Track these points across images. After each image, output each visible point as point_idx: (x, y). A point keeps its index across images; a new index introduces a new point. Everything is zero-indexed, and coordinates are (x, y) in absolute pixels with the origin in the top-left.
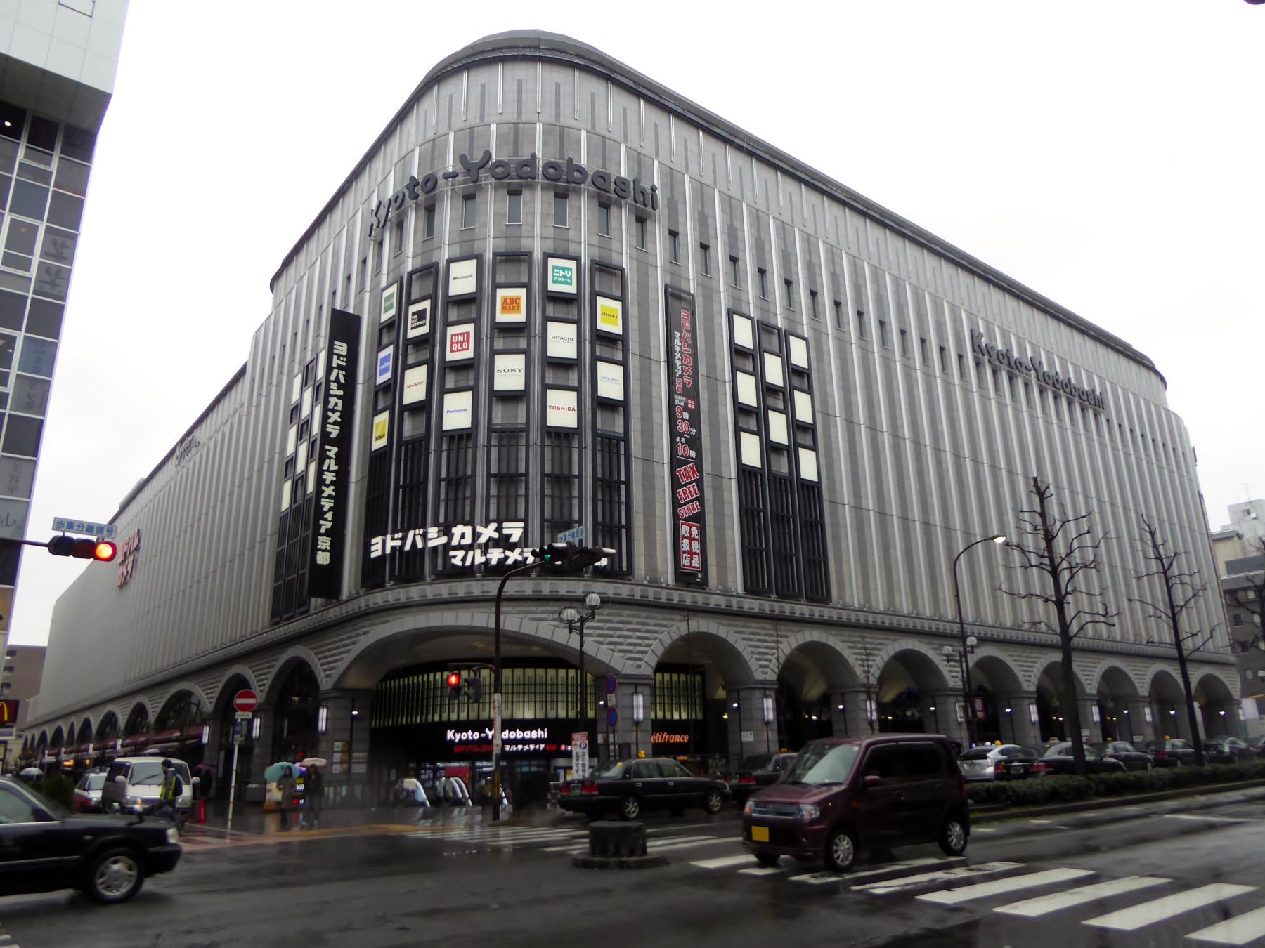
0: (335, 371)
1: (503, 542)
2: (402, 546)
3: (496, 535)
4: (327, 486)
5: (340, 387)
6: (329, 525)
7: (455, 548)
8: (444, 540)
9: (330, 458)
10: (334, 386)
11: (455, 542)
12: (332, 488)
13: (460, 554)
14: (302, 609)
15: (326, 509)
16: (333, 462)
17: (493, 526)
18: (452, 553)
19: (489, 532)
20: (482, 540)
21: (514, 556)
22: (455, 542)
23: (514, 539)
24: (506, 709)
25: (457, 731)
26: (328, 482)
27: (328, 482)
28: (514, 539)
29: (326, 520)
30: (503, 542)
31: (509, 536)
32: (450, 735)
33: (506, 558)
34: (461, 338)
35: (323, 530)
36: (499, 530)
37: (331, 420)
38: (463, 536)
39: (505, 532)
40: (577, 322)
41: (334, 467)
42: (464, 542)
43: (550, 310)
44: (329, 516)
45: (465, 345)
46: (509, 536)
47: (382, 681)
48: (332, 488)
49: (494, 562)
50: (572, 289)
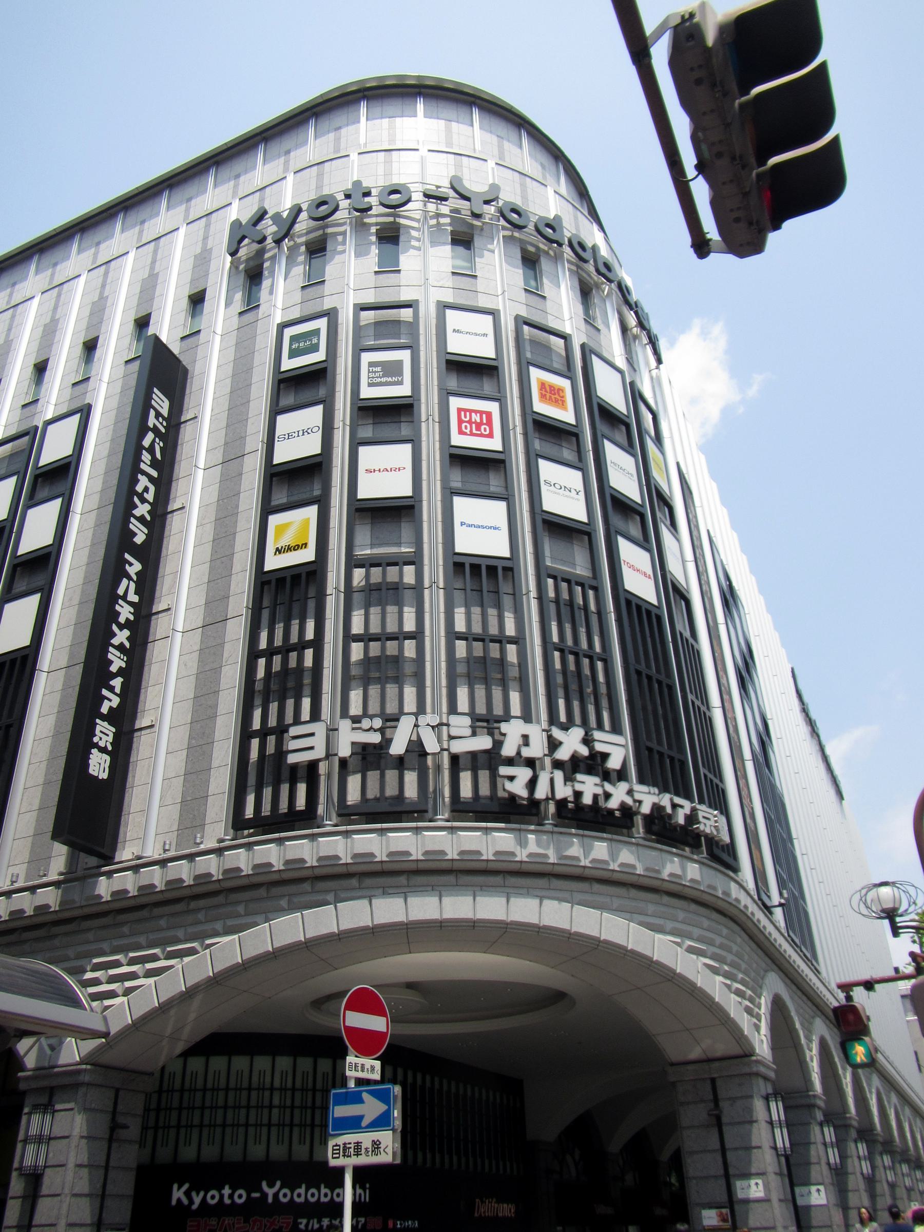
0: (150, 436)
1: (594, 763)
2: (387, 742)
3: (584, 751)
4: (121, 627)
5: (154, 464)
6: (115, 701)
7: (510, 762)
8: (484, 743)
9: (130, 578)
10: (146, 457)
11: (509, 750)
12: (126, 633)
13: (523, 774)
14: (599, 759)
15: (114, 668)
16: (133, 586)
17: (577, 733)
18: (504, 770)
19: (572, 743)
20: (563, 754)
21: (619, 795)
22: (509, 750)
23: (614, 763)
24: (301, 1141)
25: (196, 1187)
26: (122, 620)
27: (122, 620)
28: (614, 763)
29: (111, 689)
30: (594, 763)
31: (605, 756)
32: (178, 1194)
33: (608, 796)
34: (476, 418)
35: (104, 709)
36: (587, 741)
37: (137, 512)
38: (526, 739)
39: (599, 747)
40: (507, 497)
41: (133, 597)
42: (526, 753)
43: (453, 382)
44: (117, 683)
45: (485, 429)
46: (605, 756)
47: (186, 1054)
48: (126, 633)
49: (587, 800)
50: (495, 444)
